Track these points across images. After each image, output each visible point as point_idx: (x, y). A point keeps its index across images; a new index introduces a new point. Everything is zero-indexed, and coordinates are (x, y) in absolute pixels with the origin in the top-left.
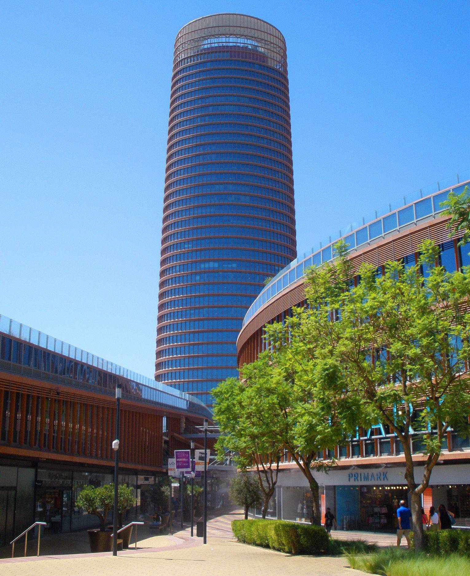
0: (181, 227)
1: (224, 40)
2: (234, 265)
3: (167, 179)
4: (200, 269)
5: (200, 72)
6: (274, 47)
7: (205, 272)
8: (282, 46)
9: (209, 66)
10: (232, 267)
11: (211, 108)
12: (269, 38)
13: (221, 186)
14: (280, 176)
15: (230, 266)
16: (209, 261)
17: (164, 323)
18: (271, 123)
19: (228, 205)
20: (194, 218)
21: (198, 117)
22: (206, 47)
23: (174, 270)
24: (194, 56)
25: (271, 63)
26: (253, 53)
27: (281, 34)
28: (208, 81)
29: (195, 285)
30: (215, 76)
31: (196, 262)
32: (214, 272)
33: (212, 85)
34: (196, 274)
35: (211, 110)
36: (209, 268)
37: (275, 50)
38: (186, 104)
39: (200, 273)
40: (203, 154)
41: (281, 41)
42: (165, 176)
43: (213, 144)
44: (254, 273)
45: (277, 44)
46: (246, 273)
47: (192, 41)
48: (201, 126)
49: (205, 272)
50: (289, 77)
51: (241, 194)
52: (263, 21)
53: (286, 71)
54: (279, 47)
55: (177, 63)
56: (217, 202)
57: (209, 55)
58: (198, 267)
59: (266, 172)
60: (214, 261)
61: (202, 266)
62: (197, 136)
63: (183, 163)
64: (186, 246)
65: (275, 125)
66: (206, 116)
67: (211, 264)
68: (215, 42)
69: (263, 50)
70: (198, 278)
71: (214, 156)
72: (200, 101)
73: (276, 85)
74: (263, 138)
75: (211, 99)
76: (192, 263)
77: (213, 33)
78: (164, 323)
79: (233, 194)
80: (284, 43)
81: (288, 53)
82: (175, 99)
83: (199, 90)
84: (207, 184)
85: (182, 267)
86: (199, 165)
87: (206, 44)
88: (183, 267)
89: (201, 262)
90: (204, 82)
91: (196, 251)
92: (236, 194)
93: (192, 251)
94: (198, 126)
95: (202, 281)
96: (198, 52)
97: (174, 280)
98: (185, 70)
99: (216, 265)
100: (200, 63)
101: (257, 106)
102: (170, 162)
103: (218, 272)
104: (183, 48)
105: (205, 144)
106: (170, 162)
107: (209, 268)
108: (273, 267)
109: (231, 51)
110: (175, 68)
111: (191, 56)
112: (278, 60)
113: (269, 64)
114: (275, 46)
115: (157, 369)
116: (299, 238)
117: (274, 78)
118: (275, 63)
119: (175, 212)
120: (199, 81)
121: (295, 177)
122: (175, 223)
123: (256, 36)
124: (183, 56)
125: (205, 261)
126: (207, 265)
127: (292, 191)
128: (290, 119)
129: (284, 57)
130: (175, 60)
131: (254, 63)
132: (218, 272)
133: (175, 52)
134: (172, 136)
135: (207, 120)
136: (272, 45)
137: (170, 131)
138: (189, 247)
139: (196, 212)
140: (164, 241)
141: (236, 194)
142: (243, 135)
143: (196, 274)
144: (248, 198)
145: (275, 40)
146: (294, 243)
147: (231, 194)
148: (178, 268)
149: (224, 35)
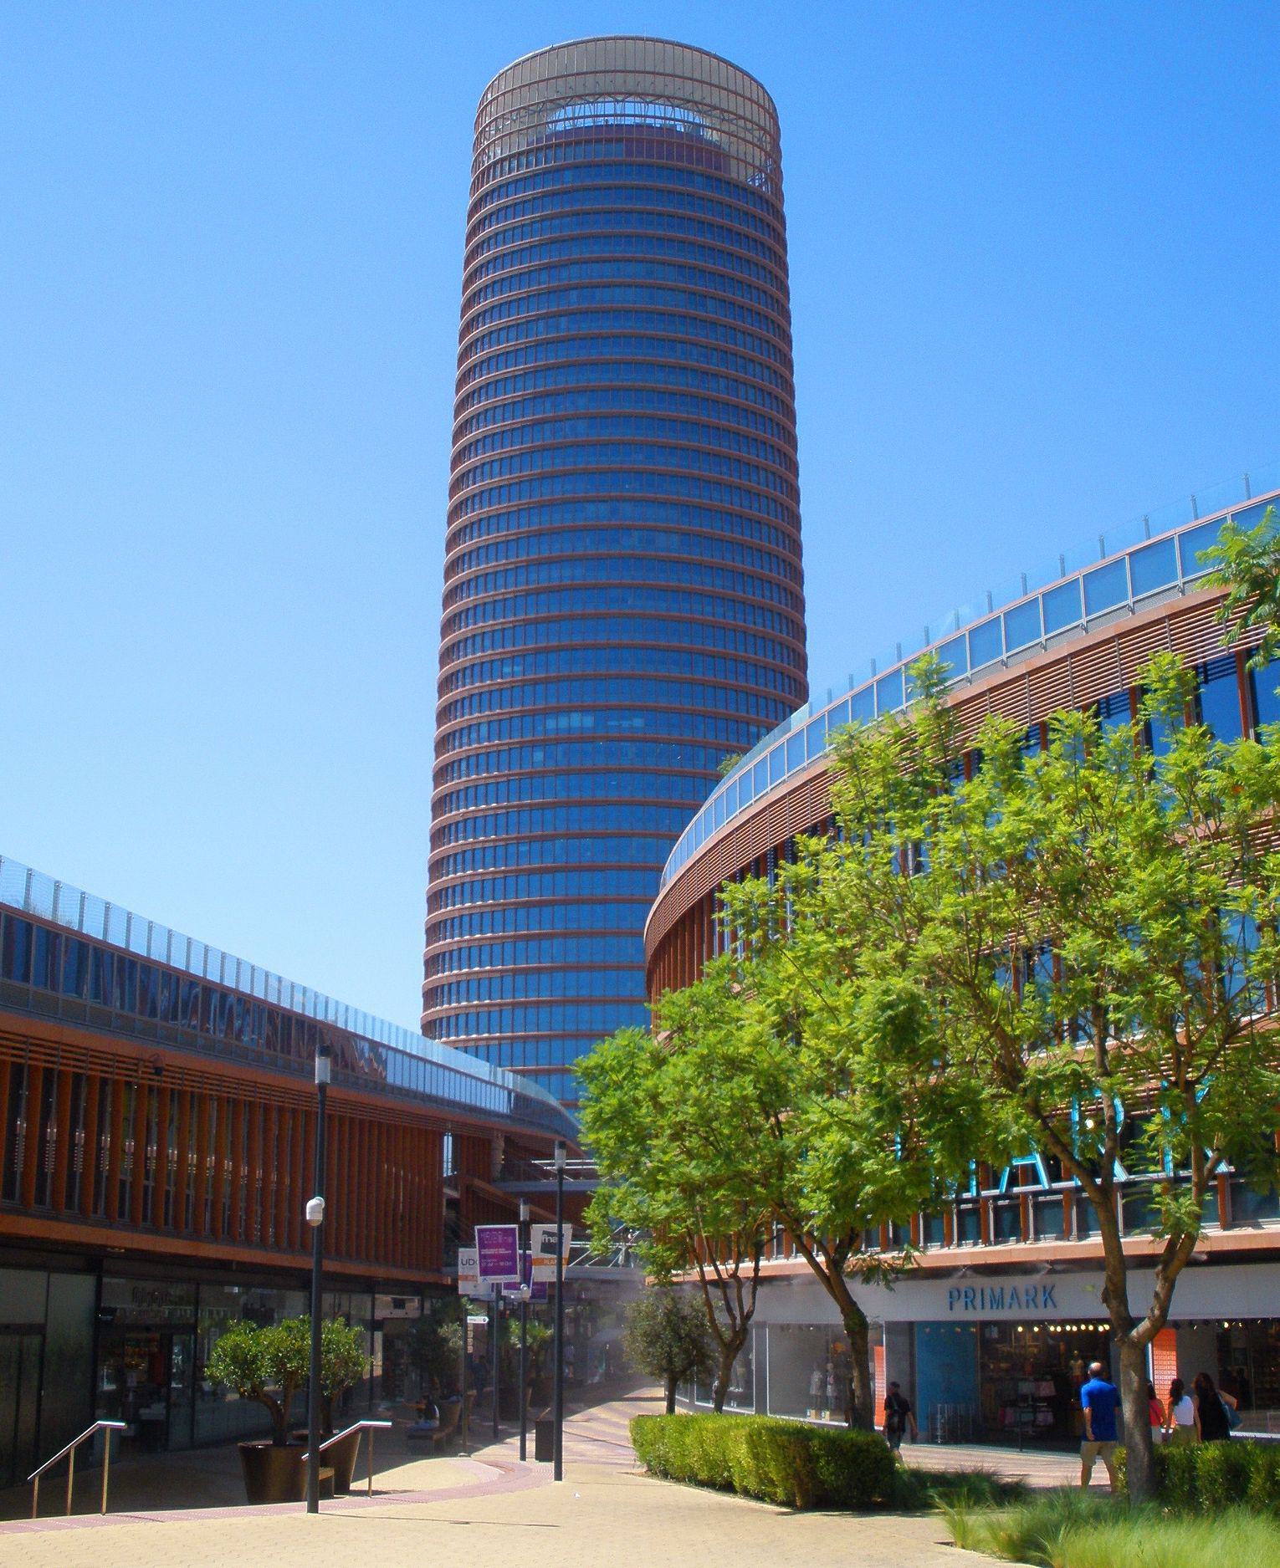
0: (494, 618)
1: (609, 108)
2: (638, 722)
3: (455, 487)
4: (545, 731)
5: (545, 195)
6: (746, 129)
7: (557, 742)
8: (768, 125)
9: (569, 180)
10: (631, 727)
11: (574, 294)
12: (732, 103)
13: (603, 507)
14: (762, 480)
15: (625, 724)
16: (569, 710)
17: (447, 879)
18: (739, 335)
19: (621, 557)
20: (528, 593)
21: (539, 318)
22: (560, 127)
23: (474, 735)
24: (528, 152)
25: (737, 173)
26: (690, 145)
27: (765, 91)
28: (566, 220)
29: (531, 775)
30: (587, 207)
31: (534, 713)
32: (582, 740)
33: (577, 232)
34: (533, 745)
35: (574, 301)
36: (570, 729)
37: (749, 137)
38: (506, 283)
39: (544, 743)
40: (554, 420)
41: (766, 111)
42: (448, 478)
43: (581, 391)
44: (693, 744)
45: (755, 119)
46: (669, 742)
47: (523, 112)
48: (548, 342)
49: (557, 742)
50: (787, 210)
51: (655, 529)
52: (716, 57)
53: (779, 194)
54: (761, 128)
55: (483, 172)
56: (592, 551)
57: (570, 150)
58: (540, 728)
59: (724, 469)
60: (583, 710)
61: (551, 723)
62: (535, 371)
63: (497, 444)
64: (507, 670)
65: (749, 339)
66: (560, 315)
67: (576, 720)
68: (585, 115)
69: (715, 136)
70: (539, 756)
71: (582, 426)
72: (544, 276)
73: (752, 232)
74: (715, 375)
75: (574, 269)
76: (523, 715)
77: (580, 91)
78: (447, 879)
79: (636, 528)
80: (774, 117)
81: (783, 144)
82: (476, 271)
83: (541, 245)
84: (564, 502)
85: (495, 726)
86: (543, 449)
87: (562, 120)
88: (498, 726)
89: (547, 712)
90: (556, 222)
91: (535, 682)
92: (641, 528)
93: (524, 683)
94: (538, 344)
95: (551, 766)
96: (539, 140)
97: (474, 761)
98: (503, 190)
99: (589, 721)
100: (546, 172)
101: (700, 289)
102: (463, 441)
103: (593, 740)
104: (497, 130)
105: (557, 393)
106: (463, 441)
107: (570, 729)
108: (743, 727)
109: (628, 140)
110: (476, 185)
111: (520, 154)
112: (757, 163)
113: (734, 175)
114: (749, 125)
115: (427, 1005)
116: (814, 648)
117: (746, 213)
118: (750, 170)
119: (477, 577)
120: (543, 219)
121: (804, 482)
122: (476, 607)
123: (697, 98)
124: (498, 153)
125: (558, 711)
126: (563, 722)
127: (795, 520)
128: (790, 323)
129: (775, 154)
130: (477, 163)
131: (691, 173)
132: (593, 740)
133: (478, 141)
134: (469, 370)
135: (565, 328)
136: (741, 122)
137: (463, 357)
138: (514, 673)
139: (533, 576)
140: (446, 656)
141: (641, 528)
142: (662, 367)
143: (533, 745)
144: (675, 538)
145: (748, 110)
146: (801, 661)
147: (629, 528)
148: (484, 729)
149: (609, 94)
